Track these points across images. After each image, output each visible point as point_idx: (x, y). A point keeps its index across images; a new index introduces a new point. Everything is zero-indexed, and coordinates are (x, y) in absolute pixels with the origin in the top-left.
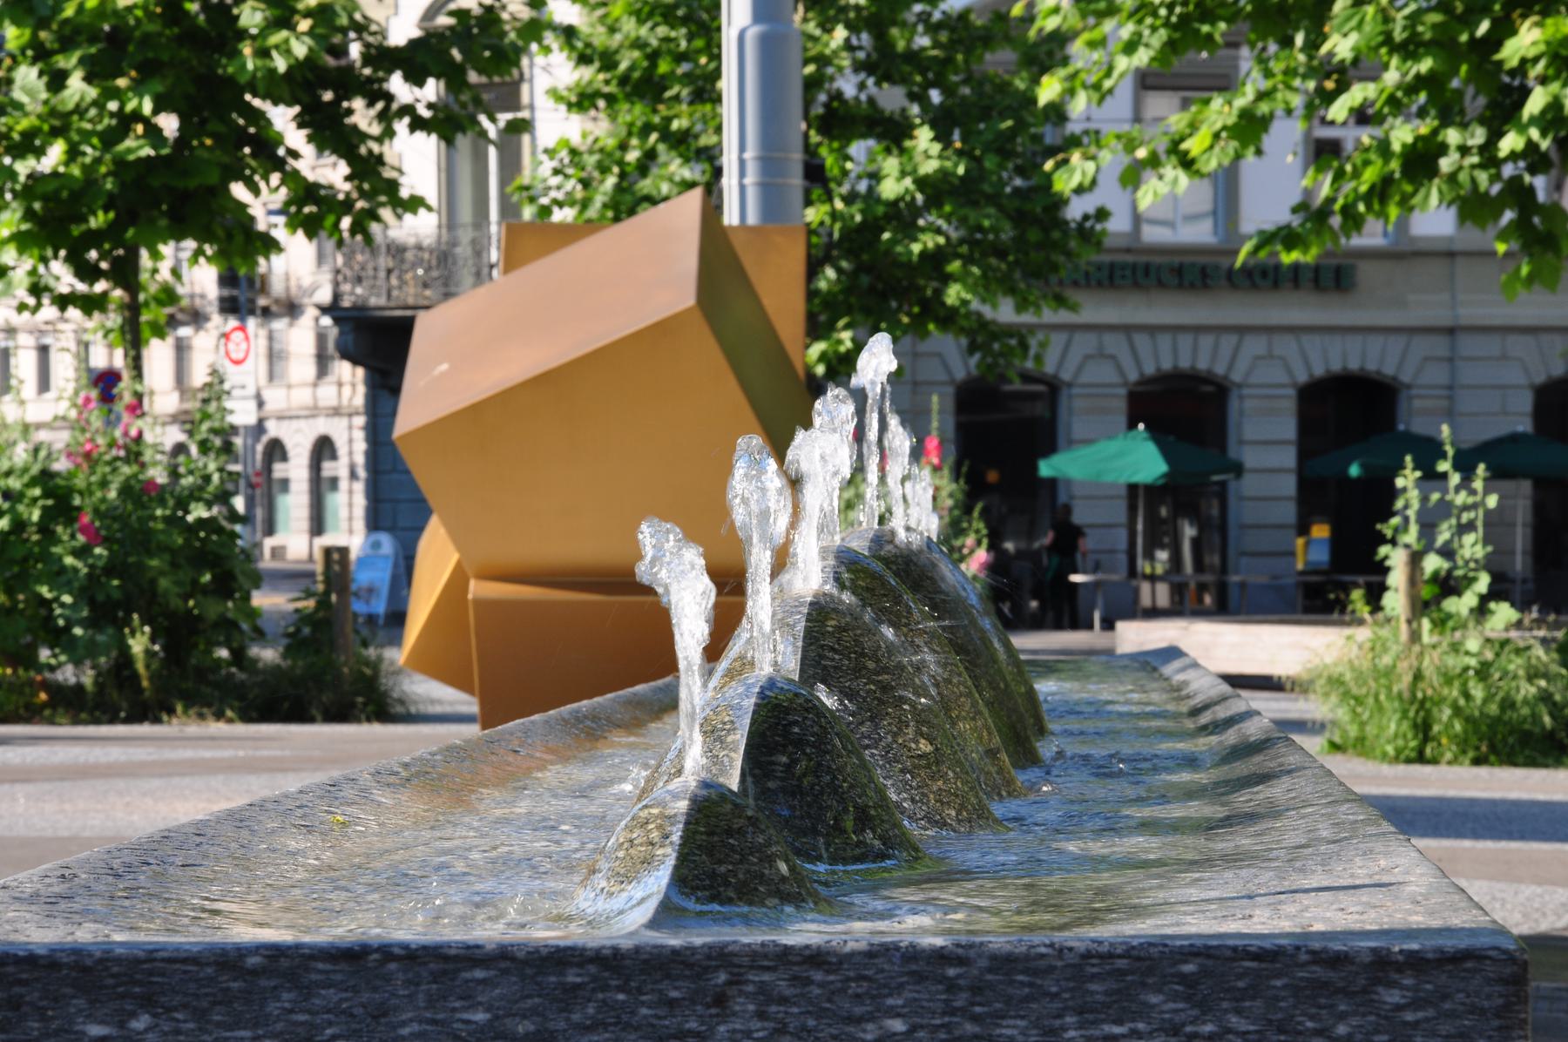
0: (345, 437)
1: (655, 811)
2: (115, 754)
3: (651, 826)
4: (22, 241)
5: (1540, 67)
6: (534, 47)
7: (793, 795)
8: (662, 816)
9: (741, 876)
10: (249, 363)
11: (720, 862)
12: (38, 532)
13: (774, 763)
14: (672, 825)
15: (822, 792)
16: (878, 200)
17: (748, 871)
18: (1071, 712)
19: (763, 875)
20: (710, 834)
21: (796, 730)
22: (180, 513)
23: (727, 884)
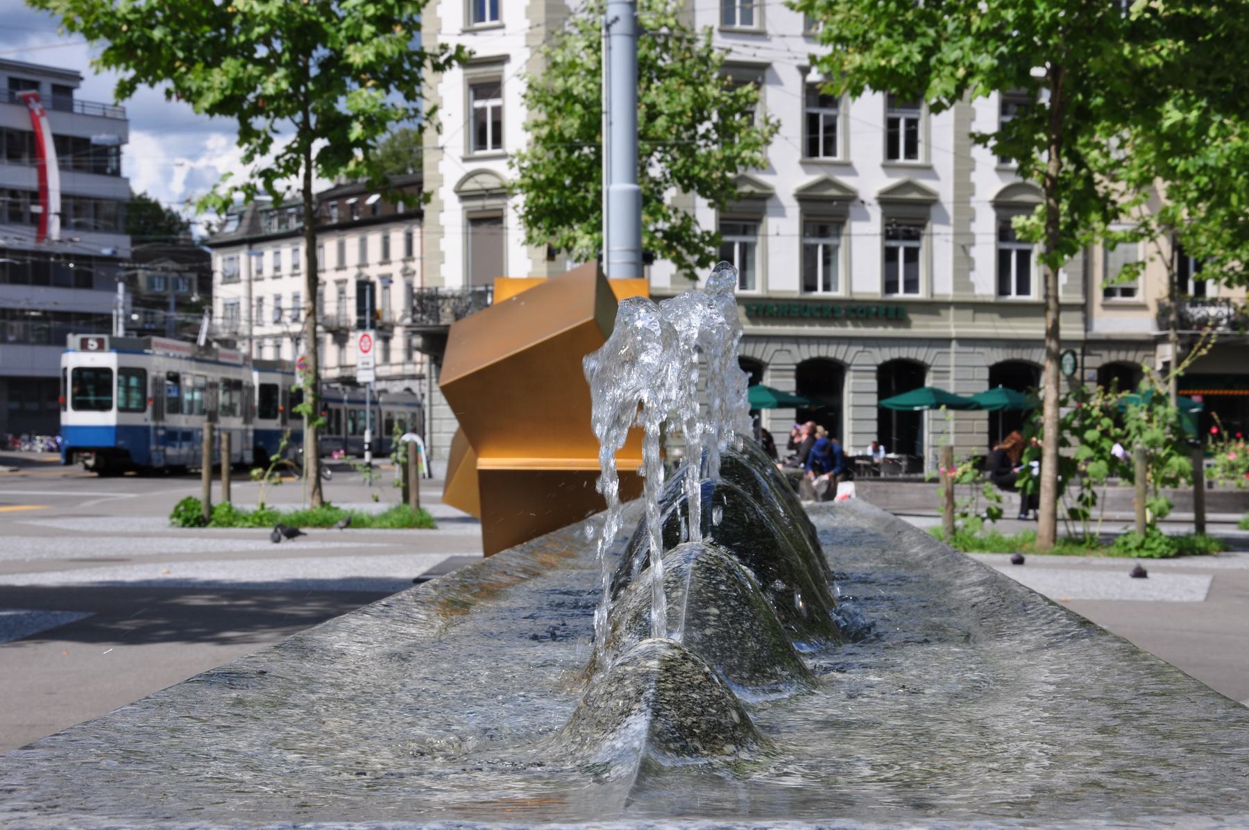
0: (434, 394)
1: (629, 669)
2: (240, 545)
3: (627, 682)
4: (285, 11)
5: (1052, 201)
6: (715, 56)
7: (723, 639)
8: (635, 673)
9: (703, 726)
10: (371, 353)
11: (686, 715)
12: (299, 218)
13: (708, 614)
14: (647, 681)
15: (743, 636)
16: (1117, 115)
17: (709, 722)
18: (841, 543)
19: (720, 724)
20: (677, 690)
21: (723, 587)
22: (1010, 41)
23: (693, 735)
